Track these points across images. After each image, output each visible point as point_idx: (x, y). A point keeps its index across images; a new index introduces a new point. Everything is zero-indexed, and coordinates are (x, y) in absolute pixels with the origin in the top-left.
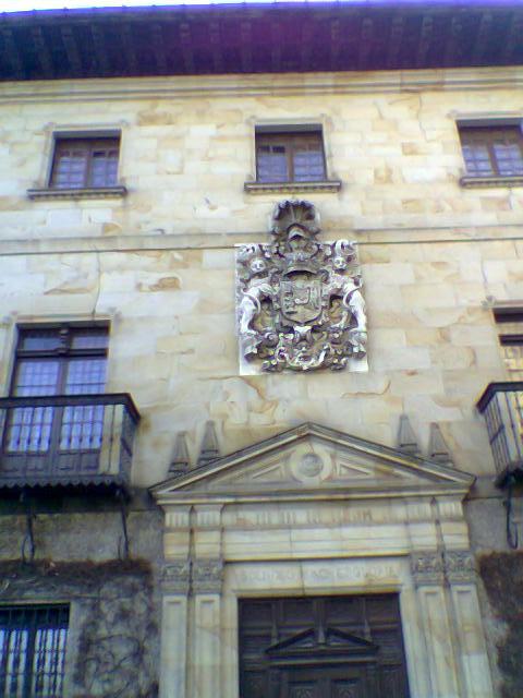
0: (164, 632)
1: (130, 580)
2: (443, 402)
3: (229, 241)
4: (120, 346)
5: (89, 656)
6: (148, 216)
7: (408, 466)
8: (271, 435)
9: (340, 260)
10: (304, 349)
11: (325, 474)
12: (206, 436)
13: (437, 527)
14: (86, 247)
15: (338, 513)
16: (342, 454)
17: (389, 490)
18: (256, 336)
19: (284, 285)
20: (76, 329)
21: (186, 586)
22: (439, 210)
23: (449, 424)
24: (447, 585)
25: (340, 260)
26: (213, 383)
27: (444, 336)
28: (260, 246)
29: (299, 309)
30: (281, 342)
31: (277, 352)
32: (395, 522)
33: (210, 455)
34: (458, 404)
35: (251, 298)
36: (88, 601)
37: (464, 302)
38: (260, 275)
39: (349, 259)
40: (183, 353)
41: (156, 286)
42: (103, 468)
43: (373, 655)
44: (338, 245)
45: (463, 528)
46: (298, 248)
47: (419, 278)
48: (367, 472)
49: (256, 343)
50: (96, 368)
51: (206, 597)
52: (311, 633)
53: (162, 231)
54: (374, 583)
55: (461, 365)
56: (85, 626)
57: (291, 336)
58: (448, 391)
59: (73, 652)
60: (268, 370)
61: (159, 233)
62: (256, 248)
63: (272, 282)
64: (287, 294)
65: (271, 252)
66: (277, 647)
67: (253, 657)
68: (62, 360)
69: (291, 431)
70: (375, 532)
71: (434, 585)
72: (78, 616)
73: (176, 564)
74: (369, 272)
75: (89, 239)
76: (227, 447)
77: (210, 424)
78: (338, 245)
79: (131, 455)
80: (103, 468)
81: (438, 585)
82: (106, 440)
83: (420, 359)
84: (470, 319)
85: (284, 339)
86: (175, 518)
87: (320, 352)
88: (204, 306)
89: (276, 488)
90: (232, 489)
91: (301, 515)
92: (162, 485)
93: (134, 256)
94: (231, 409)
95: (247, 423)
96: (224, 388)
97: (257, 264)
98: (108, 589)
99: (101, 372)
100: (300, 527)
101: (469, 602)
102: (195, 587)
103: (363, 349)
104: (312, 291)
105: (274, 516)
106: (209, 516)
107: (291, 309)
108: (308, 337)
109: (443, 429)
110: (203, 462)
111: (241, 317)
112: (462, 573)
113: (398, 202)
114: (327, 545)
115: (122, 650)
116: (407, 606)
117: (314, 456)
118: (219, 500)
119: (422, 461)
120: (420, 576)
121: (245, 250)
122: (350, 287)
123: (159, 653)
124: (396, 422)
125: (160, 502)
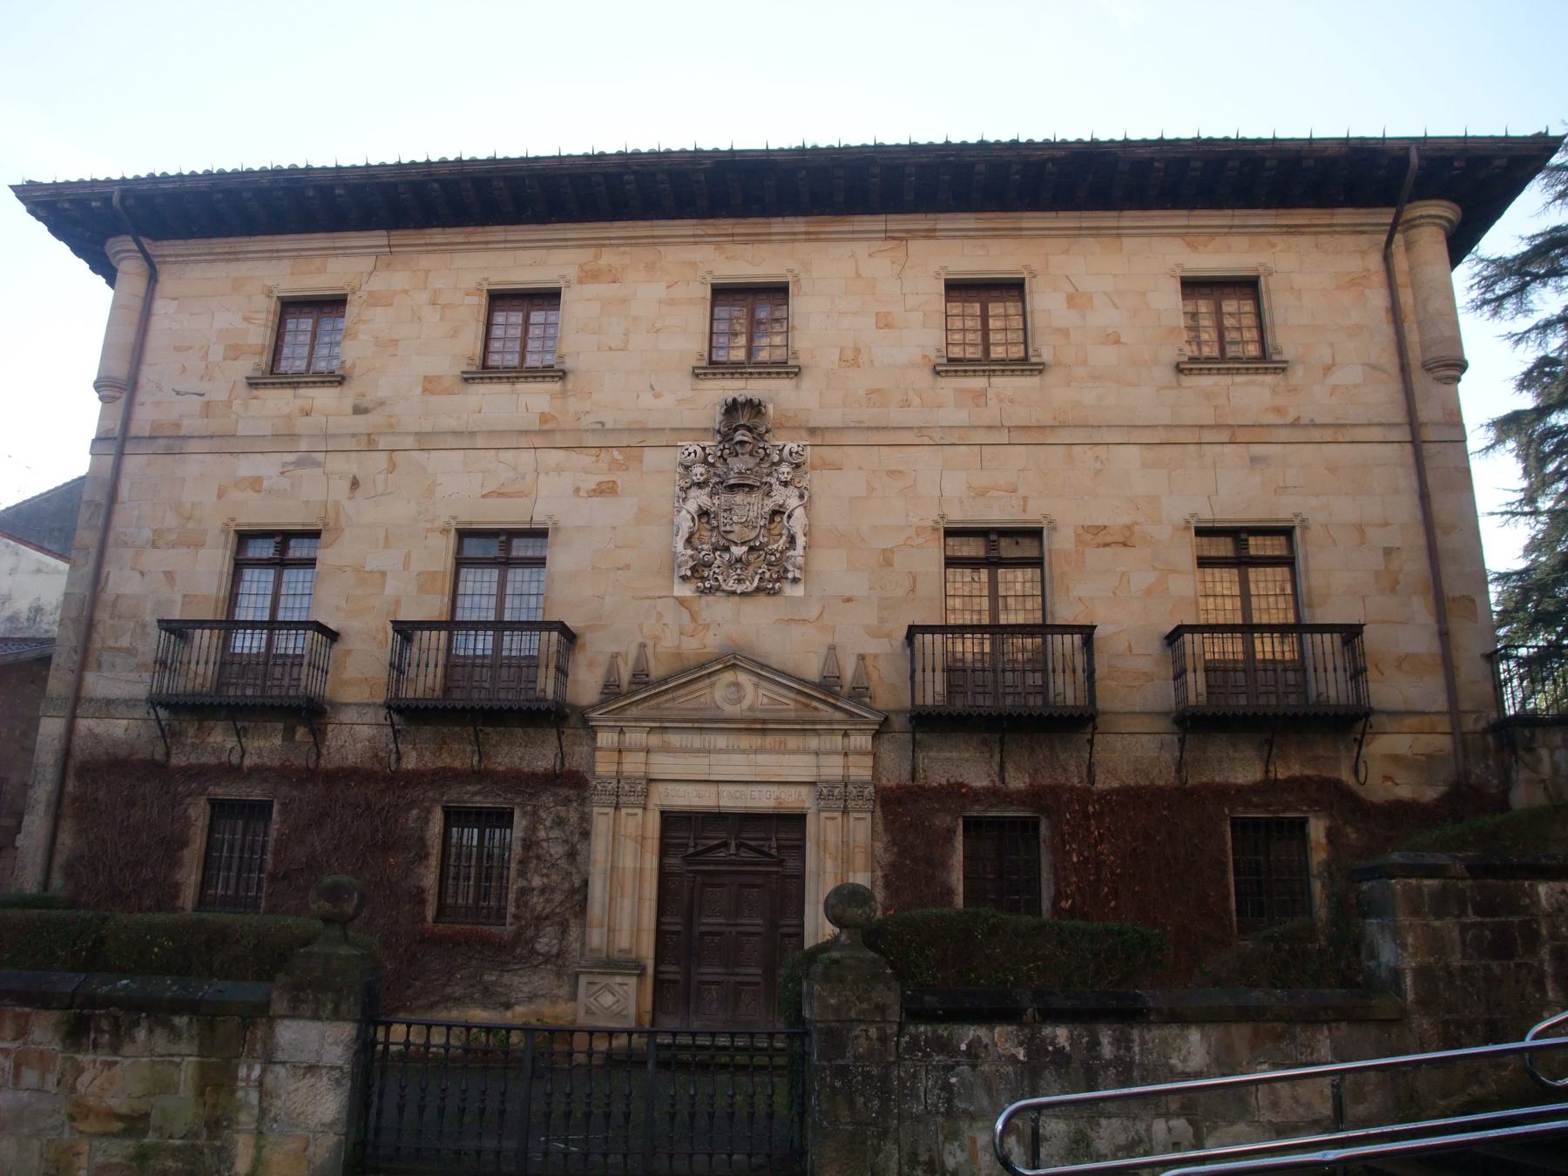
1: (564, 792)
2: (874, 633)
7: (829, 696)
11: (746, 703)
12: (638, 659)
14: (523, 442)
15: (756, 741)
16: (764, 684)
19: (724, 499)
22: (906, 403)
23: (876, 656)
24: (845, 811)
26: (647, 602)
27: (887, 558)
28: (704, 449)
29: (736, 528)
30: (717, 562)
32: (806, 752)
33: (641, 679)
34: (888, 636)
37: (915, 520)
38: (700, 485)
45: (869, 761)
48: (788, 704)
49: (691, 564)
52: (725, 845)
53: (603, 424)
59: (517, 849)
63: (711, 495)
67: (673, 861)
69: (717, 660)
72: (520, 822)
74: (817, 481)
75: (527, 432)
78: (786, 450)
84: (919, 541)
85: (720, 559)
86: (605, 739)
90: (656, 713)
91: (721, 741)
92: (593, 707)
95: (678, 647)
98: (547, 799)
100: (720, 751)
101: (861, 828)
104: (751, 507)
107: (728, 528)
109: (869, 661)
113: (861, 392)
115: (558, 850)
122: (793, 502)
124: (823, 651)
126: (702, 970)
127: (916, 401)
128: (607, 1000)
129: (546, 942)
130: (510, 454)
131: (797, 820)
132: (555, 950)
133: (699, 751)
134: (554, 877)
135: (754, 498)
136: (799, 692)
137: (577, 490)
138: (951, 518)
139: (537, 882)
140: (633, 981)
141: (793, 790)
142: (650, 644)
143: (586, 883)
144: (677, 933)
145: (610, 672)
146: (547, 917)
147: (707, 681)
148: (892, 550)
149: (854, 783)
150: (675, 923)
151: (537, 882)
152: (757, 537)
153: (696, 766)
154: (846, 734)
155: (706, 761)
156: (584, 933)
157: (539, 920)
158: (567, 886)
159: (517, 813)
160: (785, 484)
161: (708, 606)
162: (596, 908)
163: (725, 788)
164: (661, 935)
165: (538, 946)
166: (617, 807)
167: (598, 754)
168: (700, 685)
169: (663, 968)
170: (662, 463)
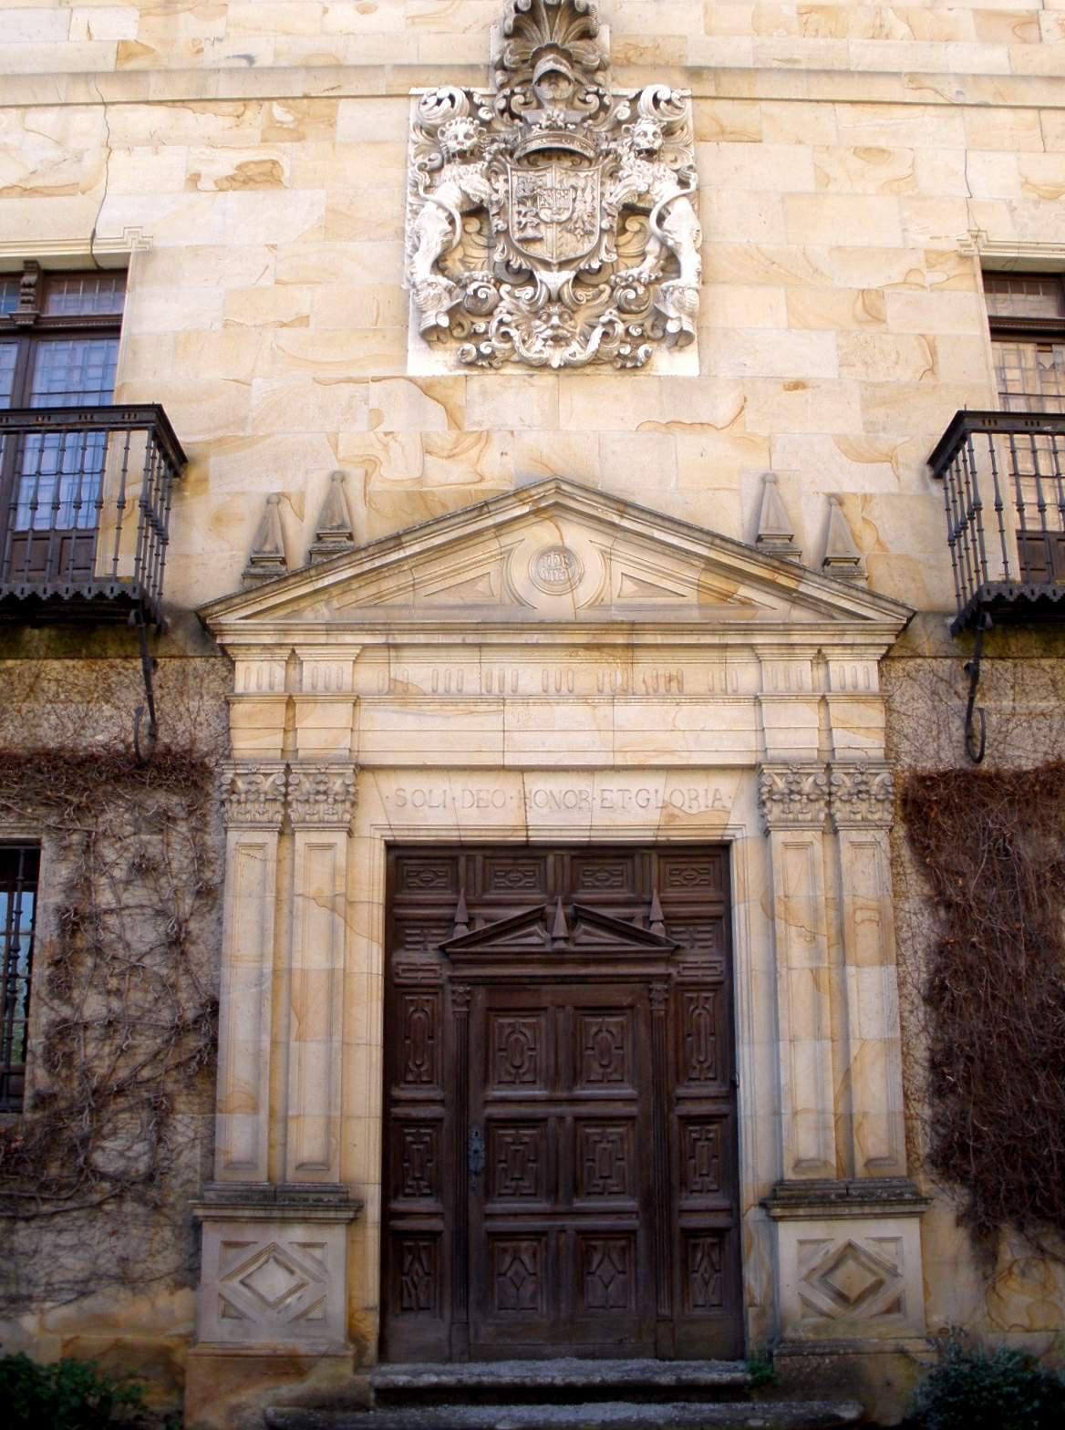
0: (228, 901)
1: (159, 800)
2: (859, 454)
3: (399, 83)
4: (147, 311)
5: (79, 943)
6: (218, 27)
7: (772, 572)
8: (470, 504)
9: (647, 131)
10: (555, 320)
11: (586, 592)
12: (329, 504)
13: (837, 708)
14: (80, 94)
15: (610, 672)
16: (625, 550)
17: (727, 628)
19: (517, 180)
20: (47, 277)
21: (275, 812)
22: (880, 32)
23: (866, 499)
24: (832, 829)
25: (647, 131)
26: (347, 389)
27: (871, 308)
28: (469, 95)
29: (549, 233)
30: (507, 303)
31: (494, 324)
32: (734, 697)
33: (334, 543)
34: (890, 458)
35: (440, 206)
36: (75, 838)
37: (922, 240)
38: (464, 156)
39: (668, 131)
40: (283, 325)
41: (232, 178)
42: (102, 569)
43: (668, 961)
44: (646, 100)
45: (876, 716)
46: (554, 101)
47: (824, 179)
48: (680, 588)
49: (447, 303)
50: (96, 358)
51: (316, 838)
52: (539, 917)
53: (250, 59)
54: (279, 1352)
55: (906, 374)
56: (70, 888)
58: (870, 426)
59: (48, 931)
60: (471, 364)
61: (244, 63)
62: (460, 97)
63: (490, 174)
64: (521, 202)
65: (492, 109)
66: (465, 942)
67: (416, 958)
68: (26, 342)
69: (518, 494)
70: (687, 715)
71: (802, 829)
72: (54, 872)
73: (254, 768)
74: (715, 162)
75: (86, 76)
76: (369, 527)
77: (338, 479)
78: (646, 100)
79: (165, 542)
80: (102, 569)
81: (813, 828)
82: (111, 508)
83: (815, 355)
84: (935, 277)
85: (512, 300)
86: (254, 674)
87: (593, 327)
88: (335, 223)
89: (476, 617)
90: (378, 615)
91: (527, 673)
92: (227, 602)
93: (186, 115)
94: (386, 447)
95: (420, 480)
96: (374, 403)
97: (460, 132)
98: (115, 816)
99: (108, 366)
100: (526, 699)
101: (868, 863)
102: (294, 816)
103: (688, 327)
104: (571, 197)
105: (463, 671)
106: (327, 667)
107: (530, 233)
108: (566, 297)
109: (853, 509)
110: (318, 559)
111: (416, 249)
112: (863, 807)
113: (789, 11)
114: (583, 740)
115: (145, 935)
116: (745, 871)
117: (564, 551)
118: (348, 639)
119: (798, 572)
120: (775, 811)
121: (433, 101)
122: (666, 189)
123: (220, 943)
124: (751, 488)
125: (228, 640)
126: (497, 1207)
127: (902, 29)
128: (275, 1282)
129: (121, 1149)
130: (50, 116)
131: (718, 852)
132: (142, 1166)
133: (479, 699)
134: (135, 996)
135: (586, 177)
136: (713, 566)
137: (194, 179)
138: (996, 237)
139: (94, 1006)
140: (335, 1238)
141: (699, 784)
142: (355, 476)
143: (212, 1008)
144: (434, 1123)
145: (263, 531)
146: (121, 1091)
147: (494, 546)
148: (880, 294)
149: (845, 764)
150: (427, 1100)
151: (94, 1006)
152: (594, 252)
153: (471, 735)
154: (820, 658)
155: (494, 722)
156: (211, 1126)
157: (103, 1096)
158: (166, 1016)
159: (46, 854)
160: (650, 154)
161: (484, 393)
162: (237, 1068)
163: (538, 784)
164: (394, 1127)
165: (99, 1159)
166: (285, 830)
167: (238, 710)
168: (478, 553)
169: (400, 1205)
170: (376, 137)
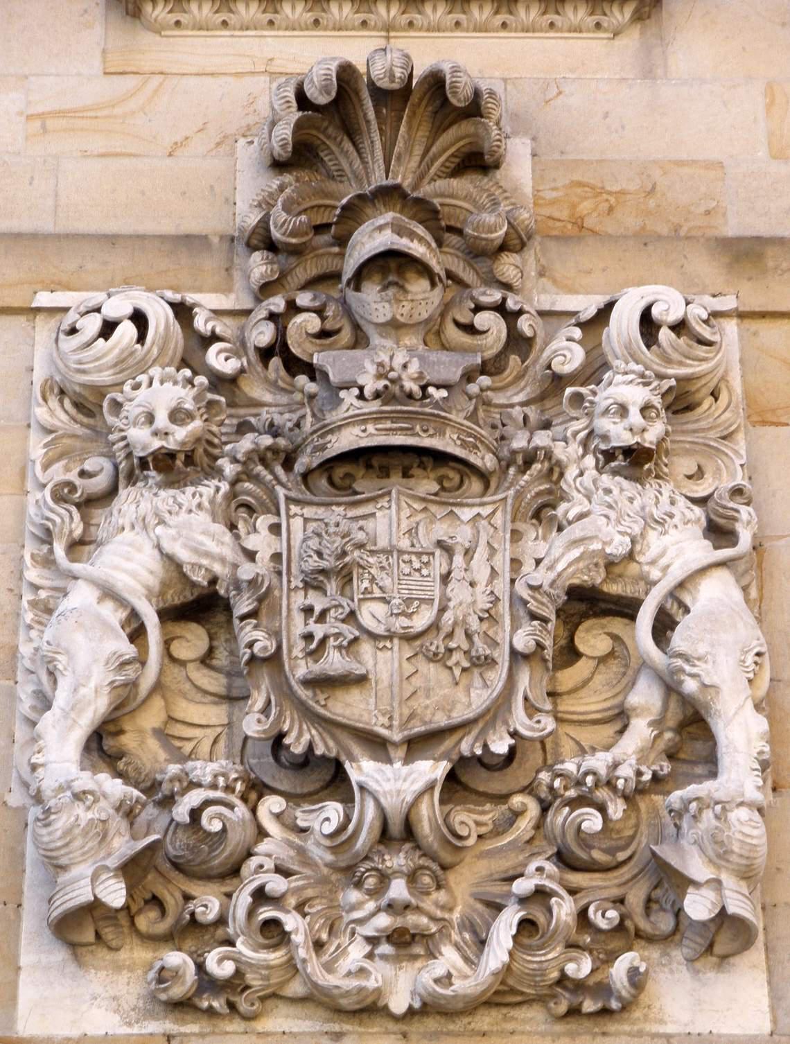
9: (626, 399)
10: (398, 890)
18: (129, 813)
19: (303, 528)
25: (626, 399)
28: (183, 312)
29: (382, 664)
30: (275, 845)
31: (244, 899)
35: (109, 593)
38: (171, 466)
39: (680, 402)
44: (625, 321)
46: (394, 326)
49: (123, 846)
57: (328, 815)
60: (182, 1006)
63: (237, 510)
64: (313, 582)
65: (240, 347)
78: (625, 321)
85: (285, 838)
87: (497, 908)
97: (159, 404)
103: (736, 906)
104: (449, 564)
107: (334, 662)
108: (425, 828)
111: (44, 702)
121: (92, 325)
122: (679, 548)
135: (475, 521)
160: (635, 461)
